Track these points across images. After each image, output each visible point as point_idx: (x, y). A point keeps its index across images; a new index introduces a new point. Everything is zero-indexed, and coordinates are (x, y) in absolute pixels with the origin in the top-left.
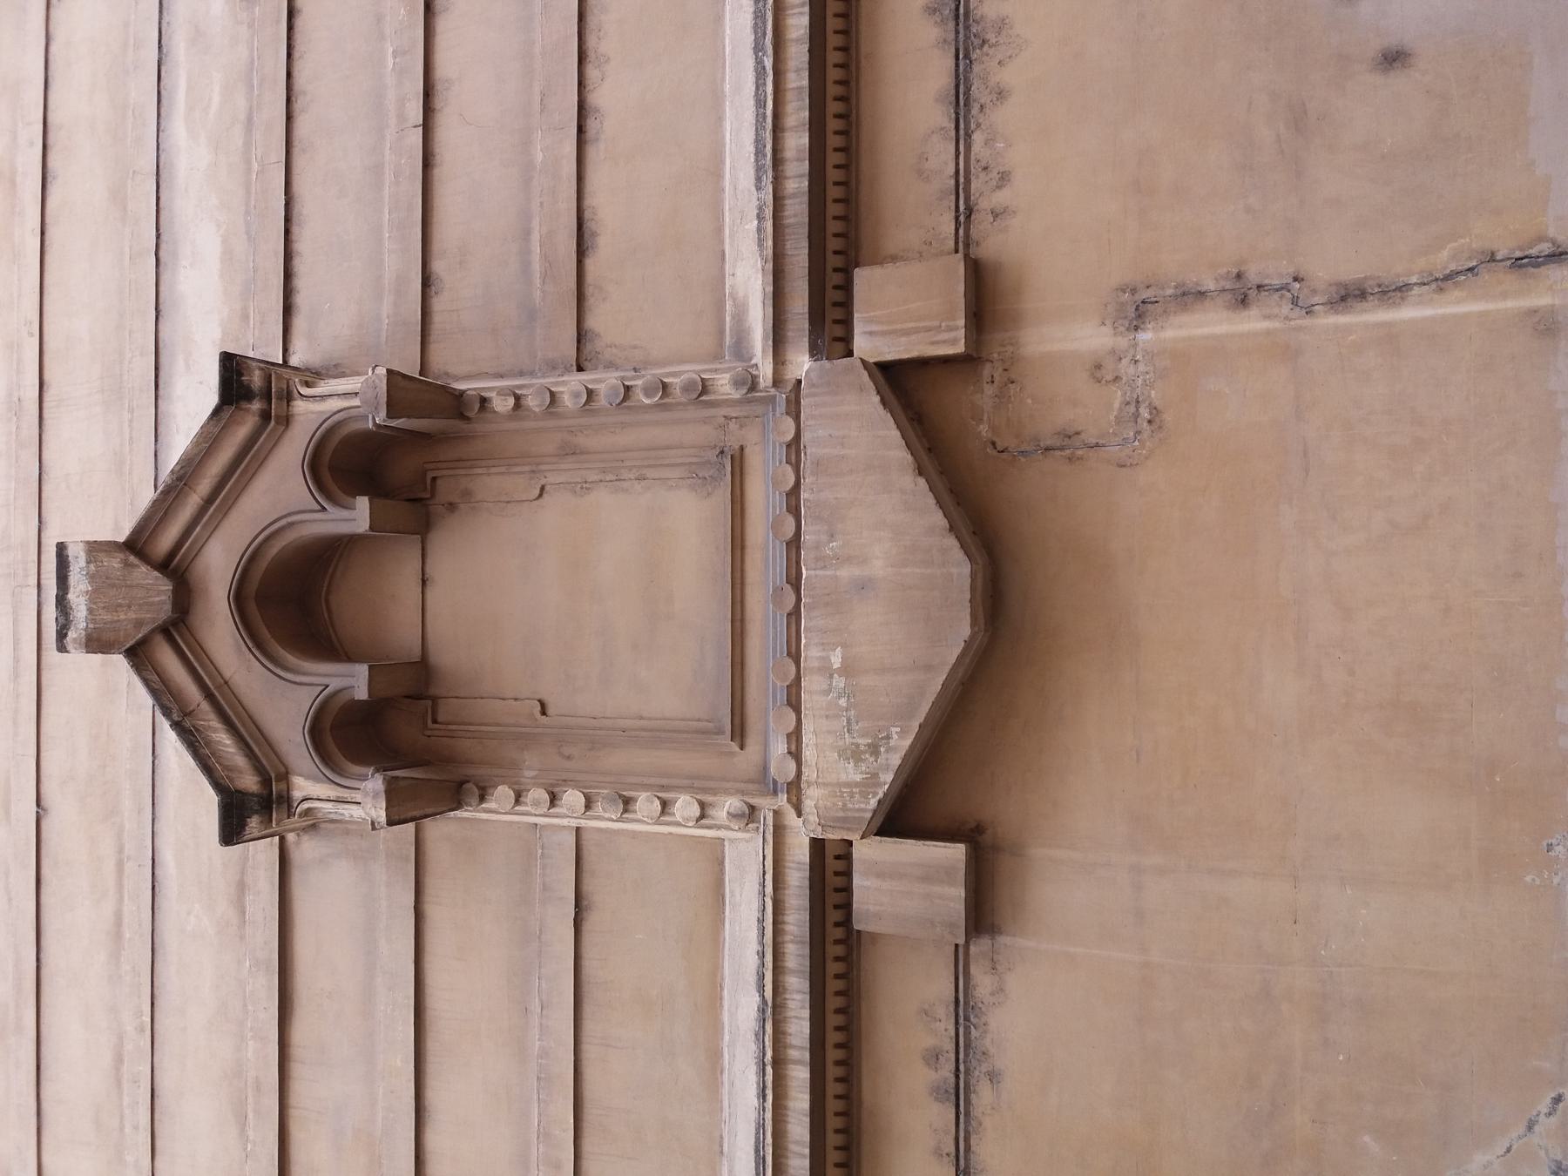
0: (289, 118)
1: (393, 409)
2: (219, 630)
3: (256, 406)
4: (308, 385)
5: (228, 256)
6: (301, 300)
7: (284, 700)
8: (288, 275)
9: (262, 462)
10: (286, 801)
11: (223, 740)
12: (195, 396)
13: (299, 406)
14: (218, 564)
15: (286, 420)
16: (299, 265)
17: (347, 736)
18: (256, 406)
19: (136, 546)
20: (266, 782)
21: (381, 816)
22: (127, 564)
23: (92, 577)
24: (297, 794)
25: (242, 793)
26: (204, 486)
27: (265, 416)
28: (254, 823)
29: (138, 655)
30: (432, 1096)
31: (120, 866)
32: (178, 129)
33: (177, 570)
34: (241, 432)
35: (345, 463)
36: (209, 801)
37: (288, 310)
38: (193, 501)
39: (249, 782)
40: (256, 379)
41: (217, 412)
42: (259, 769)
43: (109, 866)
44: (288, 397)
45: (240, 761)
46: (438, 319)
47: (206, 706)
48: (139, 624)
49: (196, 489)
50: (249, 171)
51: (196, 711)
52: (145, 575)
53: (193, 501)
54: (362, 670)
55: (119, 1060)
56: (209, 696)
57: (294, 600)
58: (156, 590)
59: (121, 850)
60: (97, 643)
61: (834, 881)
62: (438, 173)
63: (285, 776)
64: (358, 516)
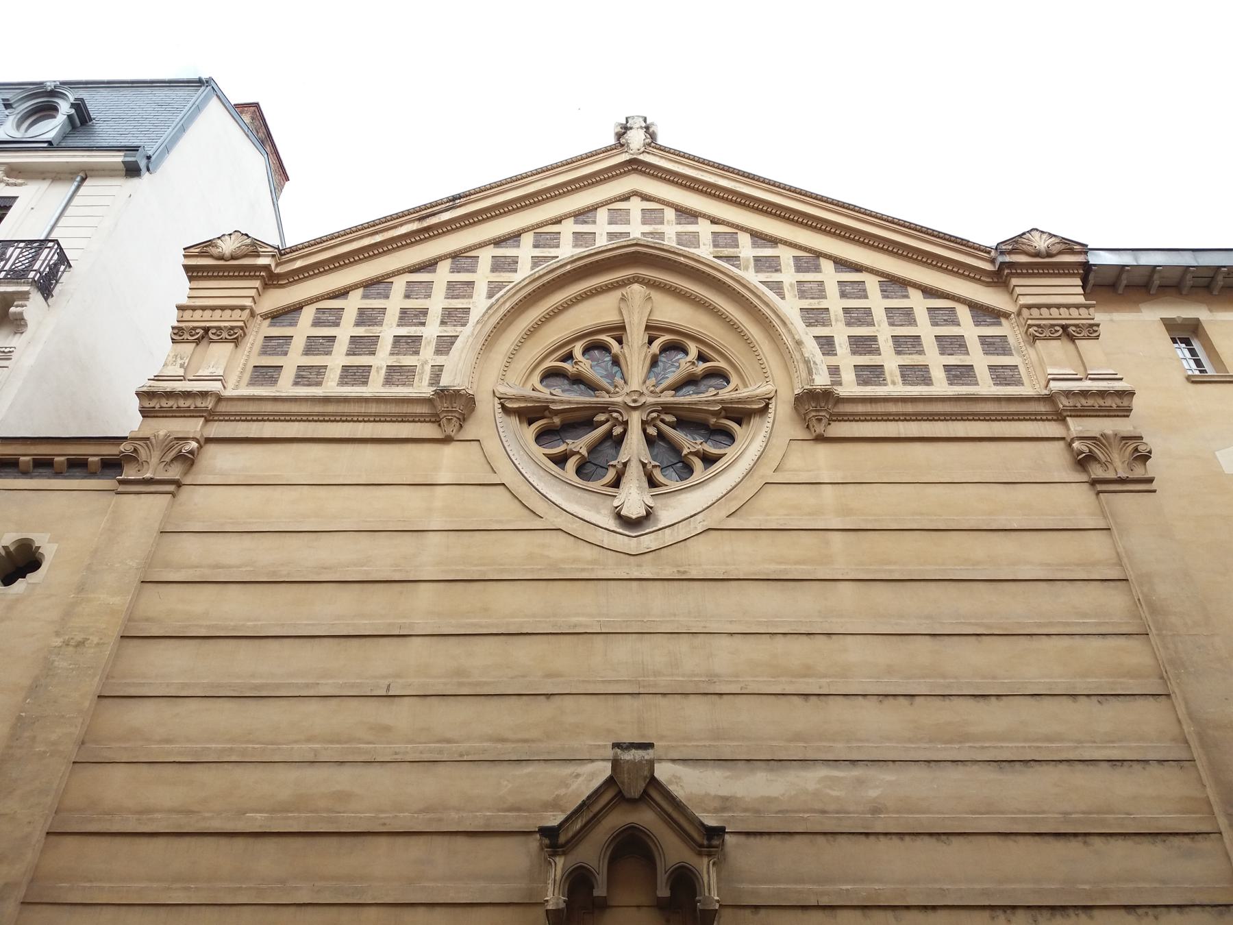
0: (825, 834)
1: (702, 911)
2: (617, 820)
3: (705, 842)
4: (714, 864)
5: (770, 800)
6: (752, 841)
7: (591, 853)
8: (761, 834)
9: (684, 840)
10: (554, 854)
11: (578, 825)
12: (711, 821)
13: (705, 860)
14: (646, 818)
15: (700, 854)
16: (765, 839)
17: (578, 881)
18: (705, 842)
19: (653, 781)
20: (562, 846)
21: (550, 907)
22: (645, 777)
23: (640, 762)
24: (557, 859)
25: (558, 836)
26: (675, 815)
27: (701, 846)
28: (547, 841)
29: (610, 781)
30: (438, 910)
31: (526, 741)
32: (823, 772)
33: (645, 797)
34: (696, 835)
35: (684, 881)
36: (555, 822)
37: (748, 834)
38: (670, 809)
39: (562, 839)
40: (715, 842)
41: (702, 824)
42: (568, 842)
43: (527, 736)
44: (709, 855)
45: (570, 834)
46: (742, 912)
47: (591, 815)
48: (623, 783)
49: (674, 811)
50: (804, 812)
51: (589, 811)
52: (642, 785)
53: (670, 809)
54: (604, 894)
55: (449, 741)
56: (595, 816)
57: (632, 848)
58: (635, 791)
59: (533, 741)
60: (616, 763)
61: (225, 335)
62: (799, 913)
63: (564, 854)
64: (664, 892)
